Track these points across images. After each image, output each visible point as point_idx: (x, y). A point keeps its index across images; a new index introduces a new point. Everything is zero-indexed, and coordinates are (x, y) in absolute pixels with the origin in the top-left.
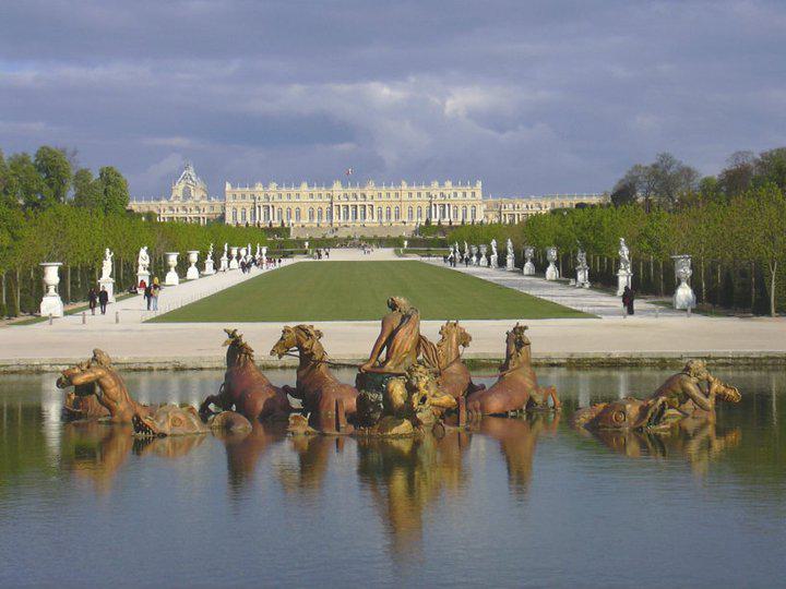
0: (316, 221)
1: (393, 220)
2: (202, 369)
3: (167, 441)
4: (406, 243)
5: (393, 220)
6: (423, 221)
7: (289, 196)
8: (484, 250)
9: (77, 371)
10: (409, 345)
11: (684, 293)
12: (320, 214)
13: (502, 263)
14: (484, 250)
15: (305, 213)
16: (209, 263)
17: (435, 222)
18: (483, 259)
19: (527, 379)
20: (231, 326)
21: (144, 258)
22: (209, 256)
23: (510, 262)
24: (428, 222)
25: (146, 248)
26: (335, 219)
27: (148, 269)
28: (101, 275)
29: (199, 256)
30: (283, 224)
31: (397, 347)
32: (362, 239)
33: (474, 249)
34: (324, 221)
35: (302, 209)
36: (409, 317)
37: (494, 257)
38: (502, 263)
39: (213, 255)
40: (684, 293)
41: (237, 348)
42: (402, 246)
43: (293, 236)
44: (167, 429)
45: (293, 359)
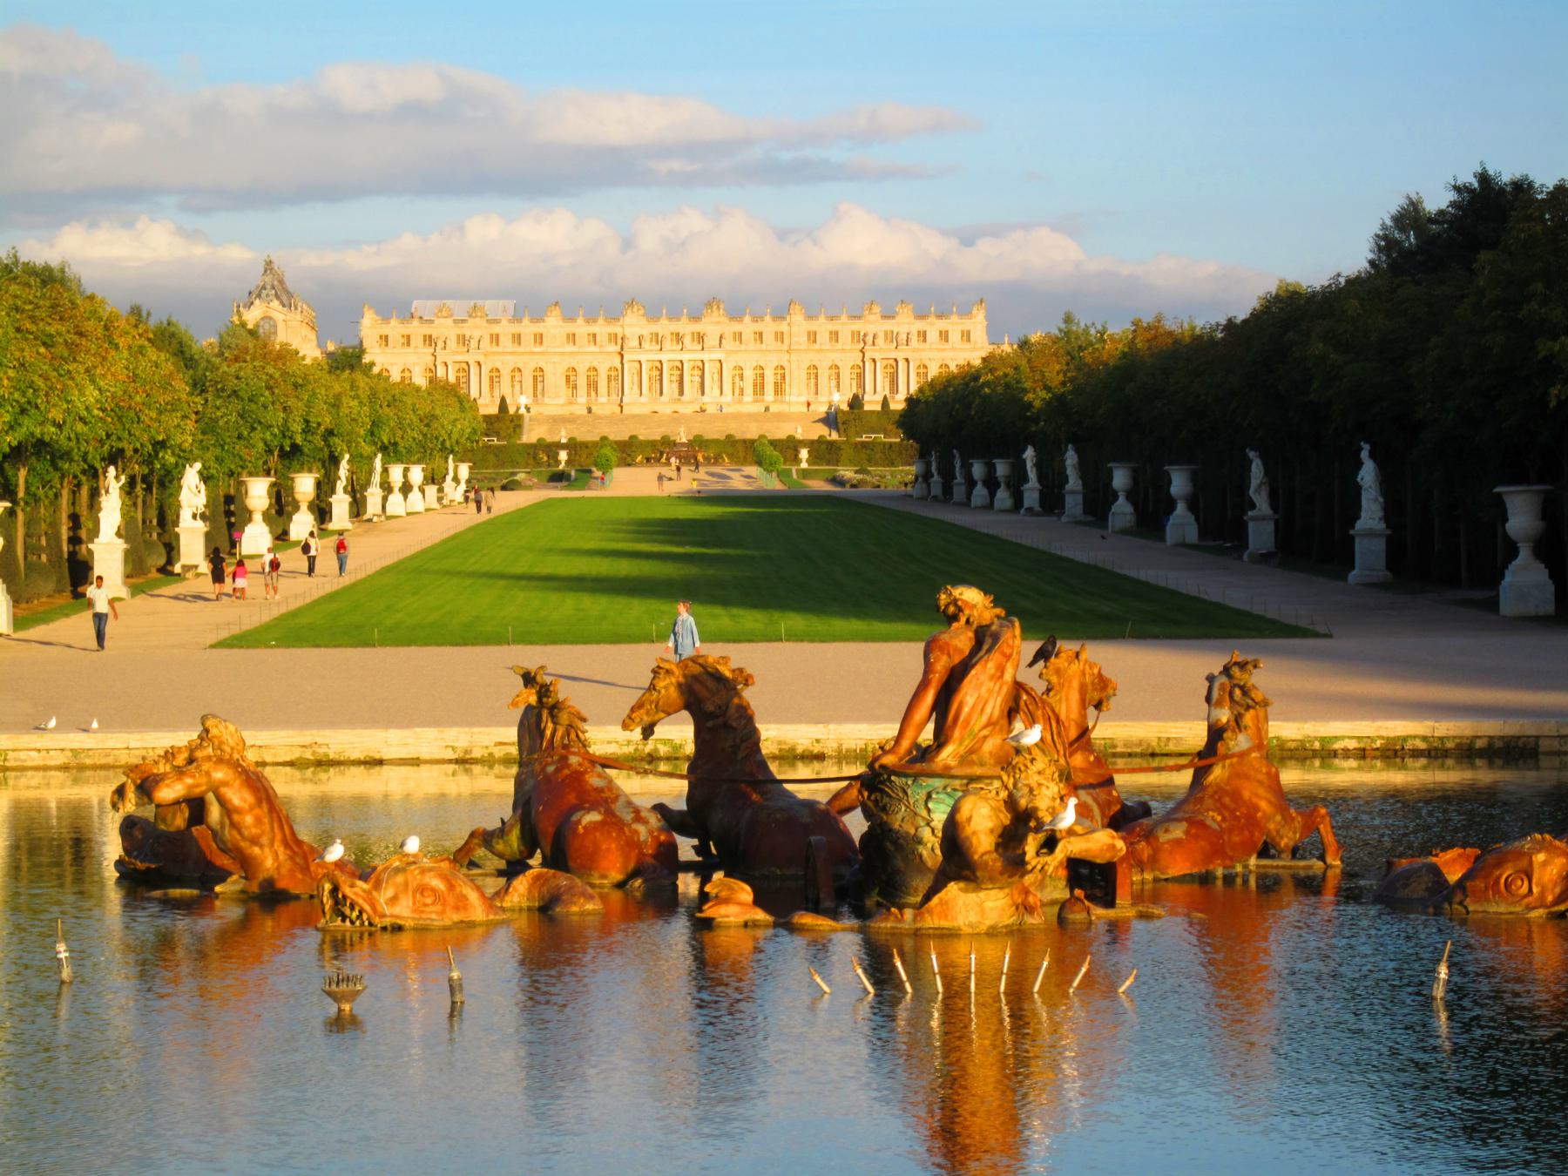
0: (582, 399)
1: (769, 395)
2: (380, 762)
3: (405, 940)
4: (804, 454)
5: (769, 395)
6: (841, 400)
7: (517, 339)
8: (1002, 469)
9: (163, 768)
10: (995, 707)
11: (1525, 580)
12: (593, 386)
13: (1052, 501)
14: (1002, 469)
15: (555, 378)
16: (340, 503)
17: (872, 403)
18: (1003, 496)
19: (1261, 791)
20: (531, 657)
21: (192, 494)
22: (340, 485)
23: (1122, 509)
24: (856, 403)
25: (198, 466)
26: (630, 394)
27: (203, 517)
28: (95, 532)
29: (319, 485)
30: (503, 405)
31: (966, 710)
32: (699, 443)
33: (978, 470)
34: (603, 399)
35: (548, 368)
36: (996, 638)
37: (1032, 491)
38: (1052, 501)
39: (351, 481)
40: (1525, 580)
41: (542, 717)
42: (796, 460)
43: (530, 436)
44: (403, 911)
45: (679, 733)
